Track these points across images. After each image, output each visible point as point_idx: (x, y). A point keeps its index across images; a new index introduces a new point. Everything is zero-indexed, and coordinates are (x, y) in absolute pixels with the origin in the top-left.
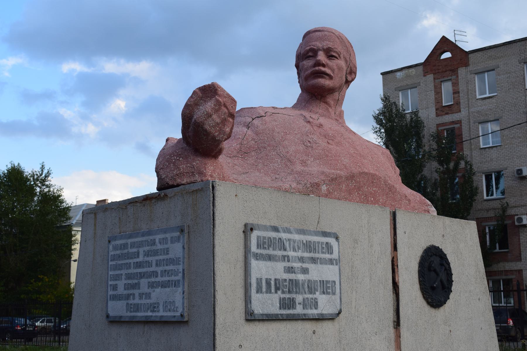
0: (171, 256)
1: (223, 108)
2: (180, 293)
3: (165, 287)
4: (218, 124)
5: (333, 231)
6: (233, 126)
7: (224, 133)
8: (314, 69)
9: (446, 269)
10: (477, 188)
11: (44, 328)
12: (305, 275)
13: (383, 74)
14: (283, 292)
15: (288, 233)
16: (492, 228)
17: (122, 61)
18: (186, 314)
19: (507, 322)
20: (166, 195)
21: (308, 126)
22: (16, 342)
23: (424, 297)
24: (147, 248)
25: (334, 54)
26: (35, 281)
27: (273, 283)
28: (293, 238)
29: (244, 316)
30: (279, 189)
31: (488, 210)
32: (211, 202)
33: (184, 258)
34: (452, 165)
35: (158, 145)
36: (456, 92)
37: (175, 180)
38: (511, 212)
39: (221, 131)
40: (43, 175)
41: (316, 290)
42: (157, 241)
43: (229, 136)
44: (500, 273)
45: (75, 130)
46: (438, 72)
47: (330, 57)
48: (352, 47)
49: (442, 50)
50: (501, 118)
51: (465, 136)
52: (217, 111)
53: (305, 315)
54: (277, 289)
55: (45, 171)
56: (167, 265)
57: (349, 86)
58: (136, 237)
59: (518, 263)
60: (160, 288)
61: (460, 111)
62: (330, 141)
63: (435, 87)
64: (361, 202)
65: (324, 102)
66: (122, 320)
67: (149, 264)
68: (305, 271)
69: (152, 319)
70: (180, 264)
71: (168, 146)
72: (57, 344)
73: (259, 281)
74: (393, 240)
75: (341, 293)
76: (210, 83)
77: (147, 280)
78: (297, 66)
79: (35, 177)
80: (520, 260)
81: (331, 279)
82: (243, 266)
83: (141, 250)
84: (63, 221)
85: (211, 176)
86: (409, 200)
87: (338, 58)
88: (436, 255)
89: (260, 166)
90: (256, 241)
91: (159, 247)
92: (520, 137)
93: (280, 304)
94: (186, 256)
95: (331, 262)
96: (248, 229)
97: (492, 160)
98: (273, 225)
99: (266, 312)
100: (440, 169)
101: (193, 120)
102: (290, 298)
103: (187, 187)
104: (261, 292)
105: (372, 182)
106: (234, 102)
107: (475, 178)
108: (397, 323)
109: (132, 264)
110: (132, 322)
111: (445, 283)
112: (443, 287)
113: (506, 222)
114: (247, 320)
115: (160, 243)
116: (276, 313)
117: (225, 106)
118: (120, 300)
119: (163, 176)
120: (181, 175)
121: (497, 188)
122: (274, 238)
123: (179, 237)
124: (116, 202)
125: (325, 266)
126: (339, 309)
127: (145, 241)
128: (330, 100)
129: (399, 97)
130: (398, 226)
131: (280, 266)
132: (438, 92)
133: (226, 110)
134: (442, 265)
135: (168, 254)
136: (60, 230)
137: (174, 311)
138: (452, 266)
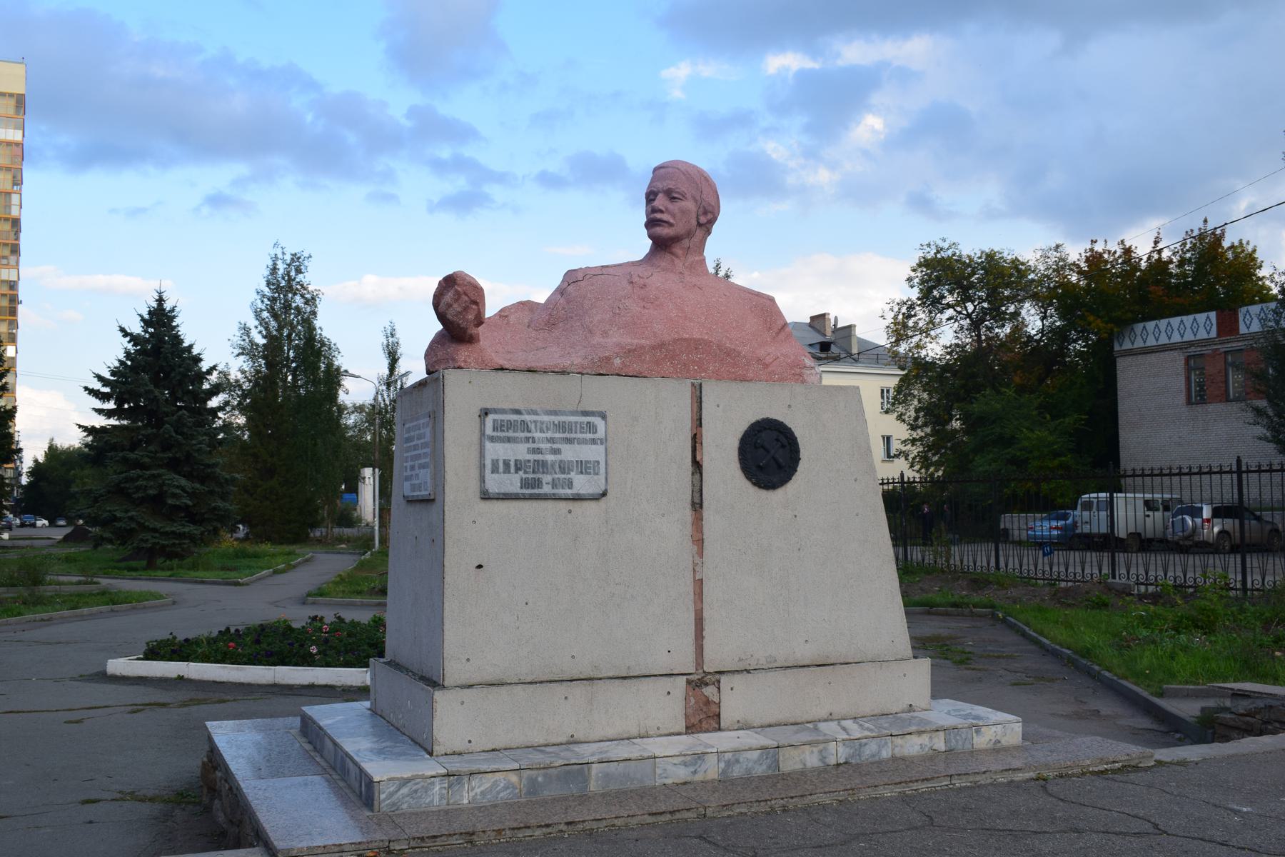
1: (463, 296)
14: (526, 472)
15: (534, 414)
27: (512, 464)
45: (791, 180)
47: (673, 199)
53: (554, 494)
68: (556, 452)
75: (606, 473)
81: (592, 458)
87: (683, 199)
93: (521, 484)
95: (594, 441)
102: (535, 478)
104: (498, 472)
108: (697, 505)
114: (482, 498)
122: (514, 421)
126: (603, 489)
133: (466, 298)
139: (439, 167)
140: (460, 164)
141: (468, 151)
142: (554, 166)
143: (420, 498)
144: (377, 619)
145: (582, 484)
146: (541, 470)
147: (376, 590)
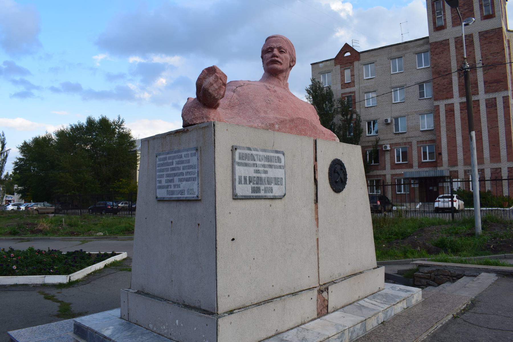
0: (190, 164)
1: (219, 80)
2: (196, 184)
3: (188, 181)
4: (216, 89)
5: (281, 150)
6: (225, 91)
7: (220, 94)
8: (271, 59)
9: (343, 172)
10: (362, 129)
11: (123, 207)
12: (266, 175)
13: (312, 64)
14: (254, 184)
16: (370, 152)
17: (164, 55)
18: (199, 196)
19: (377, 203)
20: (188, 130)
21: (268, 91)
22: (108, 215)
23: (331, 187)
24: (177, 160)
25: (283, 50)
26: (117, 182)
27: (248, 179)
28: (258, 154)
29: (232, 196)
30: (251, 127)
31: (368, 142)
32: (213, 133)
33: (198, 165)
34: (349, 117)
35: (183, 103)
36: (352, 75)
37: (193, 121)
38: (381, 143)
39: (218, 93)
40: (120, 122)
41: (272, 183)
42: (183, 156)
43: (223, 97)
44: (374, 176)
45: (137, 96)
46: (343, 64)
47: (281, 52)
48: (293, 47)
49: (345, 51)
50: (377, 90)
51: (357, 100)
52: (216, 82)
53: (265, 196)
54: (250, 182)
55: (121, 120)
56: (189, 169)
57: (291, 69)
58: (171, 153)
59: (384, 171)
60: (185, 181)
61: (355, 86)
62: (281, 100)
63: (341, 72)
64: (298, 134)
65: (277, 78)
66: (165, 199)
67: (179, 169)
68: (266, 172)
69: (181, 199)
70: (196, 168)
71: (188, 102)
72: (130, 216)
73: (240, 178)
74: (315, 155)
75: (285, 184)
76: (212, 66)
77: (178, 177)
78: (262, 57)
79: (116, 123)
80: (385, 169)
81: (280, 177)
82: (231, 169)
83: (174, 161)
84: (132, 148)
85: (213, 119)
86: (324, 134)
88: (338, 164)
89: (241, 114)
90: (238, 155)
91: (184, 159)
92: (387, 101)
93: (252, 190)
94: (199, 163)
95: (280, 167)
96: (234, 149)
97: (371, 114)
98: (248, 146)
99: (244, 194)
100: (342, 118)
101: (202, 87)
103: (199, 125)
104: (241, 184)
105: (304, 123)
106: (225, 77)
107: (361, 124)
108: (316, 201)
109: (169, 168)
110: (170, 201)
111: (343, 179)
112: (342, 181)
113: (378, 149)
114: (234, 199)
115: (185, 157)
116: (250, 195)
117: (221, 79)
118: (163, 188)
119: (186, 120)
120: (196, 118)
121: (373, 129)
122: (248, 154)
123: (195, 153)
124: (160, 134)
125: (277, 170)
127: (177, 156)
128: (281, 77)
129: (320, 77)
130: (318, 148)
131: (252, 169)
132: (343, 75)
133: (221, 81)
134: (341, 169)
135: (189, 163)
136: (131, 153)
137: (193, 194)
138: (347, 170)
139: (15, 82)
140: (23, 82)
141: (27, 78)
142: (57, 85)
143: (187, 199)
144: (31, 249)
145: (277, 191)
146: (260, 183)
147: (8, 233)
